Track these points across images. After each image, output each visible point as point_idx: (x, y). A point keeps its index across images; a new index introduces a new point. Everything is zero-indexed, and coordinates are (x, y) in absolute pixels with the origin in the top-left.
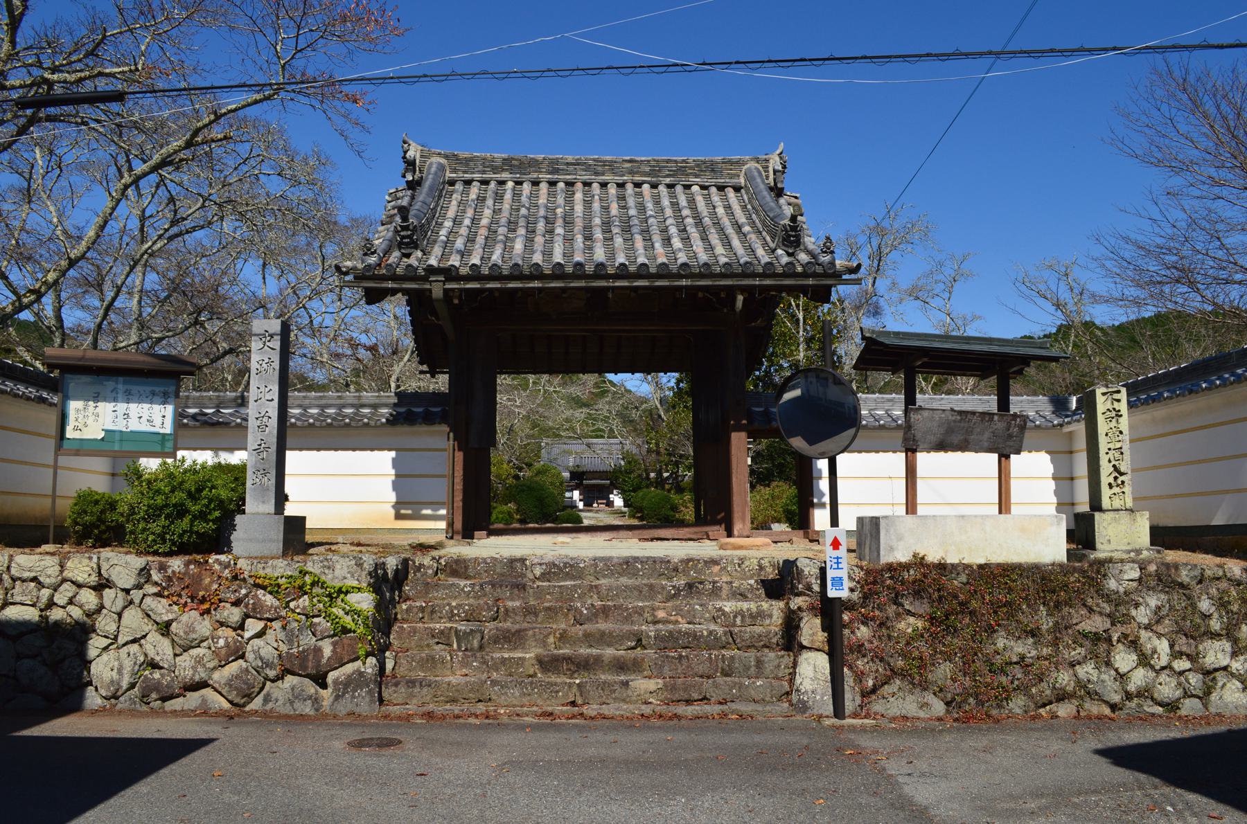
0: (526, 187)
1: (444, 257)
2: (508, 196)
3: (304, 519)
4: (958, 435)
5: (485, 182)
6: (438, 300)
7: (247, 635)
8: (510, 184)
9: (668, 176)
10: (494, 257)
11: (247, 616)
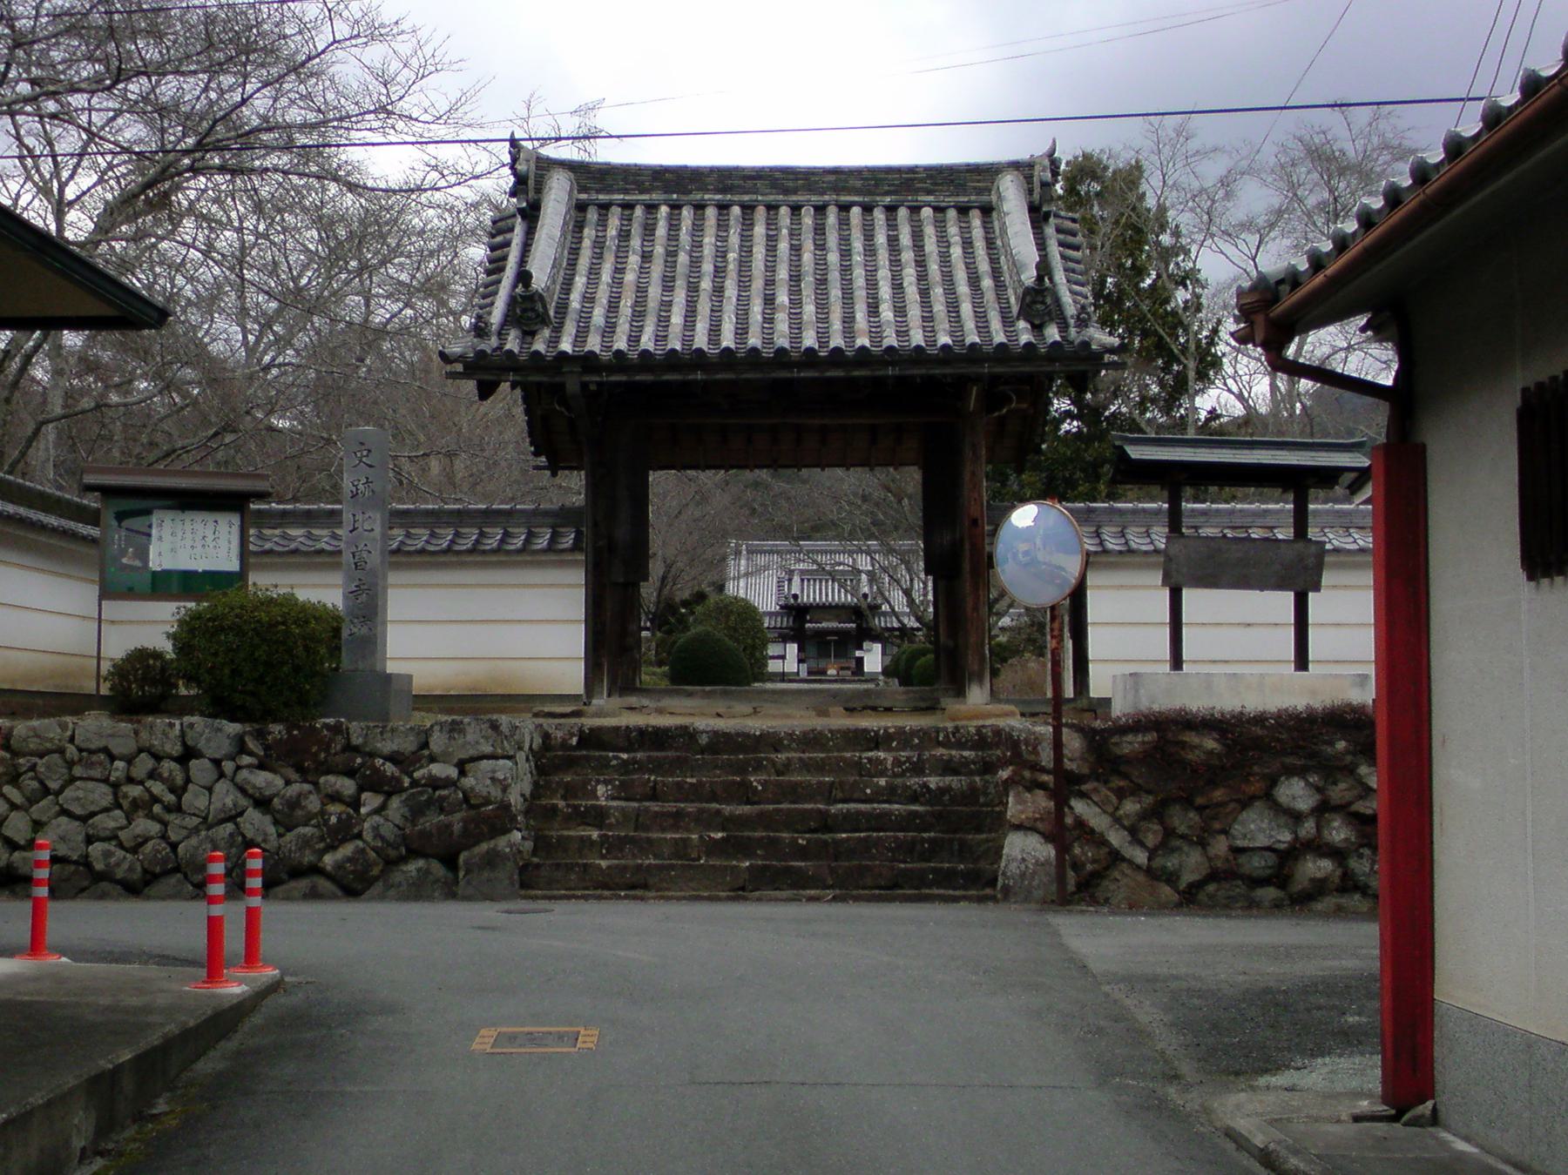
0: (687, 213)
2: (661, 231)
3: (410, 677)
5: (628, 206)
7: (363, 810)
8: (664, 209)
10: (644, 339)
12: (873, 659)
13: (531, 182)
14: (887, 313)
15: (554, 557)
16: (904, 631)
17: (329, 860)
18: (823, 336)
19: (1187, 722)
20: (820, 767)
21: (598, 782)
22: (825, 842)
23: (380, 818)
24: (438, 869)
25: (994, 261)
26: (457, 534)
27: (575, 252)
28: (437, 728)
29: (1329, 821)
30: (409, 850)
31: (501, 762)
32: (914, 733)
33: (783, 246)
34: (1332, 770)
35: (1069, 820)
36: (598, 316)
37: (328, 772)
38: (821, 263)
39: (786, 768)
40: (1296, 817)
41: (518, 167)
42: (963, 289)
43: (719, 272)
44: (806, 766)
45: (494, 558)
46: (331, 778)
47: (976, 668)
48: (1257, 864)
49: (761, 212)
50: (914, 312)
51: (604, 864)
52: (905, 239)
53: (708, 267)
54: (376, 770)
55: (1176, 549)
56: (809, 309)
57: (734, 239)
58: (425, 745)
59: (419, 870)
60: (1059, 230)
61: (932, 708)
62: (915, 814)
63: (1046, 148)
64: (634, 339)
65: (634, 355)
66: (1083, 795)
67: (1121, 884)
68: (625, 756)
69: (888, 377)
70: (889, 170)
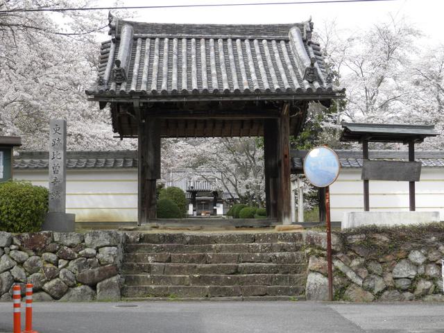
1: (138, 85)
2: (166, 47)
3: (74, 215)
4: (388, 172)
5: (153, 39)
6: (136, 108)
7: (60, 267)
8: (167, 40)
9: (250, 34)
11: (59, 258)
12: (220, 210)
13: (117, 29)
14: (254, 77)
15: (124, 170)
16: (233, 200)
17: (46, 286)
18: (230, 85)
19: (375, 230)
20: (234, 249)
21: (149, 255)
22: (238, 278)
23: (68, 270)
24: (89, 289)
25: (291, 59)
26: (88, 161)
27: (134, 54)
28: (88, 234)
29: (429, 267)
30: (78, 282)
31: (113, 248)
32: (268, 236)
33: (212, 53)
34: (430, 247)
35: (333, 268)
36: (144, 78)
37: (46, 251)
38: (227, 59)
39: (221, 249)
40: (417, 265)
41: (111, 24)
42: (281, 69)
43: (189, 62)
44: (228, 249)
45: (102, 170)
46: (47, 254)
47: (287, 211)
48: (403, 284)
49: (203, 41)
50: (264, 77)
51: (153, 287)
52: (258, 51)
53: (184, 60)
54: (65, 251)
55: (368, 165)
56: (224, 76)
57: (193, 50)
58: (84, 241)
59: (82, 290)
60: (314, 49)
61: (267, 226)
62: (271, 267)
63: (308, 19)
64: (159, 86)
65: (160, 92)
66: (337, 258)
67: (352, 293)
68: (158, 245)
69: (256, 101)
70: (250, 26)
